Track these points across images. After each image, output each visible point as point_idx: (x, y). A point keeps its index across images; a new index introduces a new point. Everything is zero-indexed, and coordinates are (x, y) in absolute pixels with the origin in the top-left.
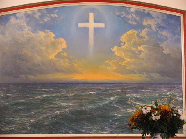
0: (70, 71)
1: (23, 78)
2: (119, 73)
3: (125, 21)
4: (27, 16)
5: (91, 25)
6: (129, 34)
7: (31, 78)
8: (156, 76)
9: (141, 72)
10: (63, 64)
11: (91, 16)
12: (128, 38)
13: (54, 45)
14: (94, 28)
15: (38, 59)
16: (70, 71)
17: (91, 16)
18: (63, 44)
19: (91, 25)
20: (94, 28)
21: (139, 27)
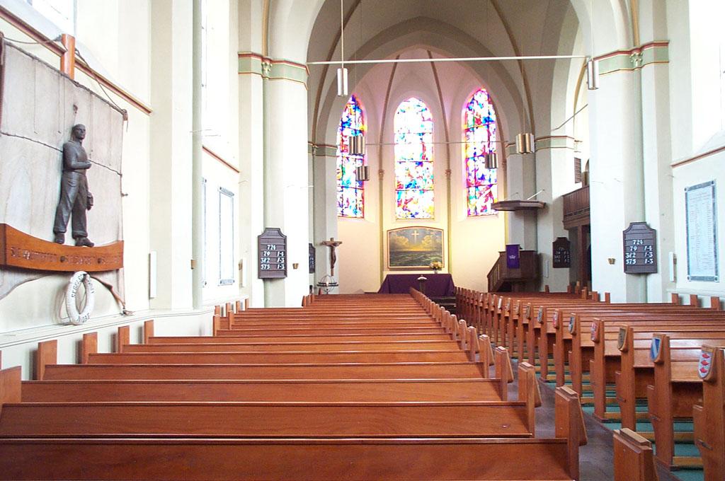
0: (408, 248)
1: (395, 251)
2: (468, 36)
3: (425, 233)
4: (397, 232)
5: (416, 234)
6: (432, 145)
7: (399, 250)
8: (435, 250)
9: (431, 247)
10: (406, 246)
11: (415, 232)
12: (687, 302)
13: (405, 240)
14: (554, 267)
15: (400, 245)
16: (408, 248)
17: (415, 232)
18: (407, 240)
19: (416, 234)
20: (554, 267)
21: (430, 234)
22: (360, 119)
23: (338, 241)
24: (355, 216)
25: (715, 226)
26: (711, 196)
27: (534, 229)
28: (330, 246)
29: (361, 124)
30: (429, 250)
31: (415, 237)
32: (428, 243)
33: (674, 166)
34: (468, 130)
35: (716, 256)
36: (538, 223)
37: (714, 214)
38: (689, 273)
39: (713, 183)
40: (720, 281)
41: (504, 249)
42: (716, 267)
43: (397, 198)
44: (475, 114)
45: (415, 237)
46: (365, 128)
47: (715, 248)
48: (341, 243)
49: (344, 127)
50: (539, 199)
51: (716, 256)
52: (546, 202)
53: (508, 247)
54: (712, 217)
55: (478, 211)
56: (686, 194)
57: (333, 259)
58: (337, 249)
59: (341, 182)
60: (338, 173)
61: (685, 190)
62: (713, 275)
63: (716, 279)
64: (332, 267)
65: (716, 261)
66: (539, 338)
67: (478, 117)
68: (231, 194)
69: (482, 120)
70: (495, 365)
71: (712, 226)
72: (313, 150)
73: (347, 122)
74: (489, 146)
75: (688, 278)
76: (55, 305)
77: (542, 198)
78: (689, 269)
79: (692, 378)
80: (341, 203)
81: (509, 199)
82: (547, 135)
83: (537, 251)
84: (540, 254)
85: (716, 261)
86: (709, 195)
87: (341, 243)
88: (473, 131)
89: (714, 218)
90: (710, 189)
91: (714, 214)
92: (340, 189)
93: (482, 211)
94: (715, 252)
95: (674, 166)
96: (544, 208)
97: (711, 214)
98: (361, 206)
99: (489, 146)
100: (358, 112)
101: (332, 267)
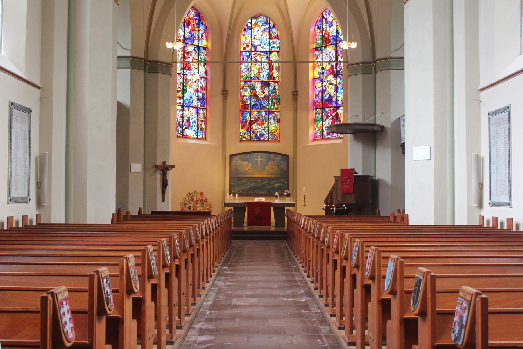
0: (253, 174)
3: (270, 158)
5: (259, 159)
10: (251, 171)
13: (248, 166)
15: (243, 170)
19: (259, 159)
22: (204, 36)
23: (171, 164)
24: (195, 136)
25: (509, 152)
26: (507, 122)
27: (373, 155)
28: (162, 170)
29: (204, 41)
30: (273, 176)
31: (259, 161)
32: (273, 169)
33: (482, 90)
34: (316, 49)
35: (510, 181)
36: (377, 148)
37: (509, 139)
38: (490, 199)
39: (508, 108)
40: (513, 206)
41: (339, 174)
42: (510, 192)
43: (241, 118)
44: (324, 32)
45: (259, 161)
46: (209, 45)
47: (509, 173)
48: (173, 167)
49: (187, 44)
50: (378, 122)
51: (510, 181)
52: (384, 125)
53: (343, 171)
54: (507, 142)
55: (325, 132)
56: (490, 118)
57: (165, 184)
58: (171, 175)
59: (181, 101)
60: (178, 92)
61: (489, 114)
62: (507, 200)
63: (509, 204)
64: (163, 192)
65: (510, 185)
66: (328, 265)
67: (327, 36)
68: (28, 111)
69: (331, 39)
70: (141, 277)
71: (507, 152)
72: (145, 67)
73: (190, 39)
74: (336, 67)
75: (490, 204)
76: (242, 289)
77: (381, 121)
78: (490, 194)
79: (32, 253)
80: (181, 123)
81: (349, 122)
82: (175, 61)
83: (375, 176)
84: (378, 180)
85: (510, 185)
86: (505, 121)
87: (173, 167)
88: (322, 51)
89: (509, 143)
90: (506, 114)
91: (509, 139)
92: (179, 108)
93: (328, 134)
94: (509, 178)
95: (482, 90)
96: (382, 131)
97: (507, 139)
98: (203, 126)
99: (336, 67)
100: (202, 28)
101: (163, 192)
